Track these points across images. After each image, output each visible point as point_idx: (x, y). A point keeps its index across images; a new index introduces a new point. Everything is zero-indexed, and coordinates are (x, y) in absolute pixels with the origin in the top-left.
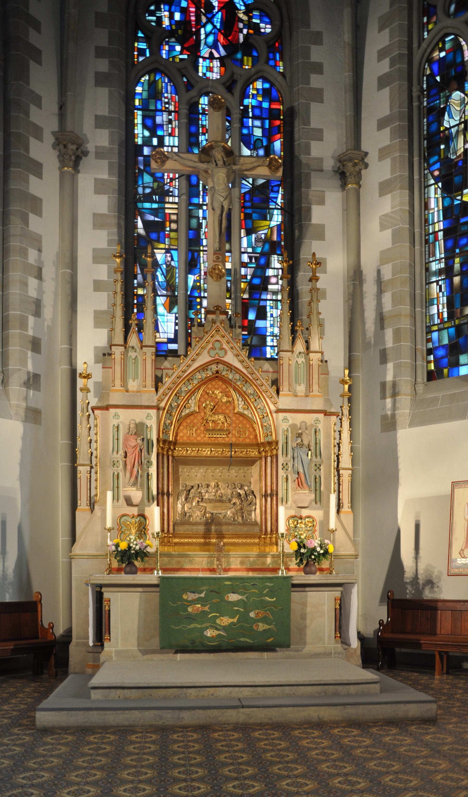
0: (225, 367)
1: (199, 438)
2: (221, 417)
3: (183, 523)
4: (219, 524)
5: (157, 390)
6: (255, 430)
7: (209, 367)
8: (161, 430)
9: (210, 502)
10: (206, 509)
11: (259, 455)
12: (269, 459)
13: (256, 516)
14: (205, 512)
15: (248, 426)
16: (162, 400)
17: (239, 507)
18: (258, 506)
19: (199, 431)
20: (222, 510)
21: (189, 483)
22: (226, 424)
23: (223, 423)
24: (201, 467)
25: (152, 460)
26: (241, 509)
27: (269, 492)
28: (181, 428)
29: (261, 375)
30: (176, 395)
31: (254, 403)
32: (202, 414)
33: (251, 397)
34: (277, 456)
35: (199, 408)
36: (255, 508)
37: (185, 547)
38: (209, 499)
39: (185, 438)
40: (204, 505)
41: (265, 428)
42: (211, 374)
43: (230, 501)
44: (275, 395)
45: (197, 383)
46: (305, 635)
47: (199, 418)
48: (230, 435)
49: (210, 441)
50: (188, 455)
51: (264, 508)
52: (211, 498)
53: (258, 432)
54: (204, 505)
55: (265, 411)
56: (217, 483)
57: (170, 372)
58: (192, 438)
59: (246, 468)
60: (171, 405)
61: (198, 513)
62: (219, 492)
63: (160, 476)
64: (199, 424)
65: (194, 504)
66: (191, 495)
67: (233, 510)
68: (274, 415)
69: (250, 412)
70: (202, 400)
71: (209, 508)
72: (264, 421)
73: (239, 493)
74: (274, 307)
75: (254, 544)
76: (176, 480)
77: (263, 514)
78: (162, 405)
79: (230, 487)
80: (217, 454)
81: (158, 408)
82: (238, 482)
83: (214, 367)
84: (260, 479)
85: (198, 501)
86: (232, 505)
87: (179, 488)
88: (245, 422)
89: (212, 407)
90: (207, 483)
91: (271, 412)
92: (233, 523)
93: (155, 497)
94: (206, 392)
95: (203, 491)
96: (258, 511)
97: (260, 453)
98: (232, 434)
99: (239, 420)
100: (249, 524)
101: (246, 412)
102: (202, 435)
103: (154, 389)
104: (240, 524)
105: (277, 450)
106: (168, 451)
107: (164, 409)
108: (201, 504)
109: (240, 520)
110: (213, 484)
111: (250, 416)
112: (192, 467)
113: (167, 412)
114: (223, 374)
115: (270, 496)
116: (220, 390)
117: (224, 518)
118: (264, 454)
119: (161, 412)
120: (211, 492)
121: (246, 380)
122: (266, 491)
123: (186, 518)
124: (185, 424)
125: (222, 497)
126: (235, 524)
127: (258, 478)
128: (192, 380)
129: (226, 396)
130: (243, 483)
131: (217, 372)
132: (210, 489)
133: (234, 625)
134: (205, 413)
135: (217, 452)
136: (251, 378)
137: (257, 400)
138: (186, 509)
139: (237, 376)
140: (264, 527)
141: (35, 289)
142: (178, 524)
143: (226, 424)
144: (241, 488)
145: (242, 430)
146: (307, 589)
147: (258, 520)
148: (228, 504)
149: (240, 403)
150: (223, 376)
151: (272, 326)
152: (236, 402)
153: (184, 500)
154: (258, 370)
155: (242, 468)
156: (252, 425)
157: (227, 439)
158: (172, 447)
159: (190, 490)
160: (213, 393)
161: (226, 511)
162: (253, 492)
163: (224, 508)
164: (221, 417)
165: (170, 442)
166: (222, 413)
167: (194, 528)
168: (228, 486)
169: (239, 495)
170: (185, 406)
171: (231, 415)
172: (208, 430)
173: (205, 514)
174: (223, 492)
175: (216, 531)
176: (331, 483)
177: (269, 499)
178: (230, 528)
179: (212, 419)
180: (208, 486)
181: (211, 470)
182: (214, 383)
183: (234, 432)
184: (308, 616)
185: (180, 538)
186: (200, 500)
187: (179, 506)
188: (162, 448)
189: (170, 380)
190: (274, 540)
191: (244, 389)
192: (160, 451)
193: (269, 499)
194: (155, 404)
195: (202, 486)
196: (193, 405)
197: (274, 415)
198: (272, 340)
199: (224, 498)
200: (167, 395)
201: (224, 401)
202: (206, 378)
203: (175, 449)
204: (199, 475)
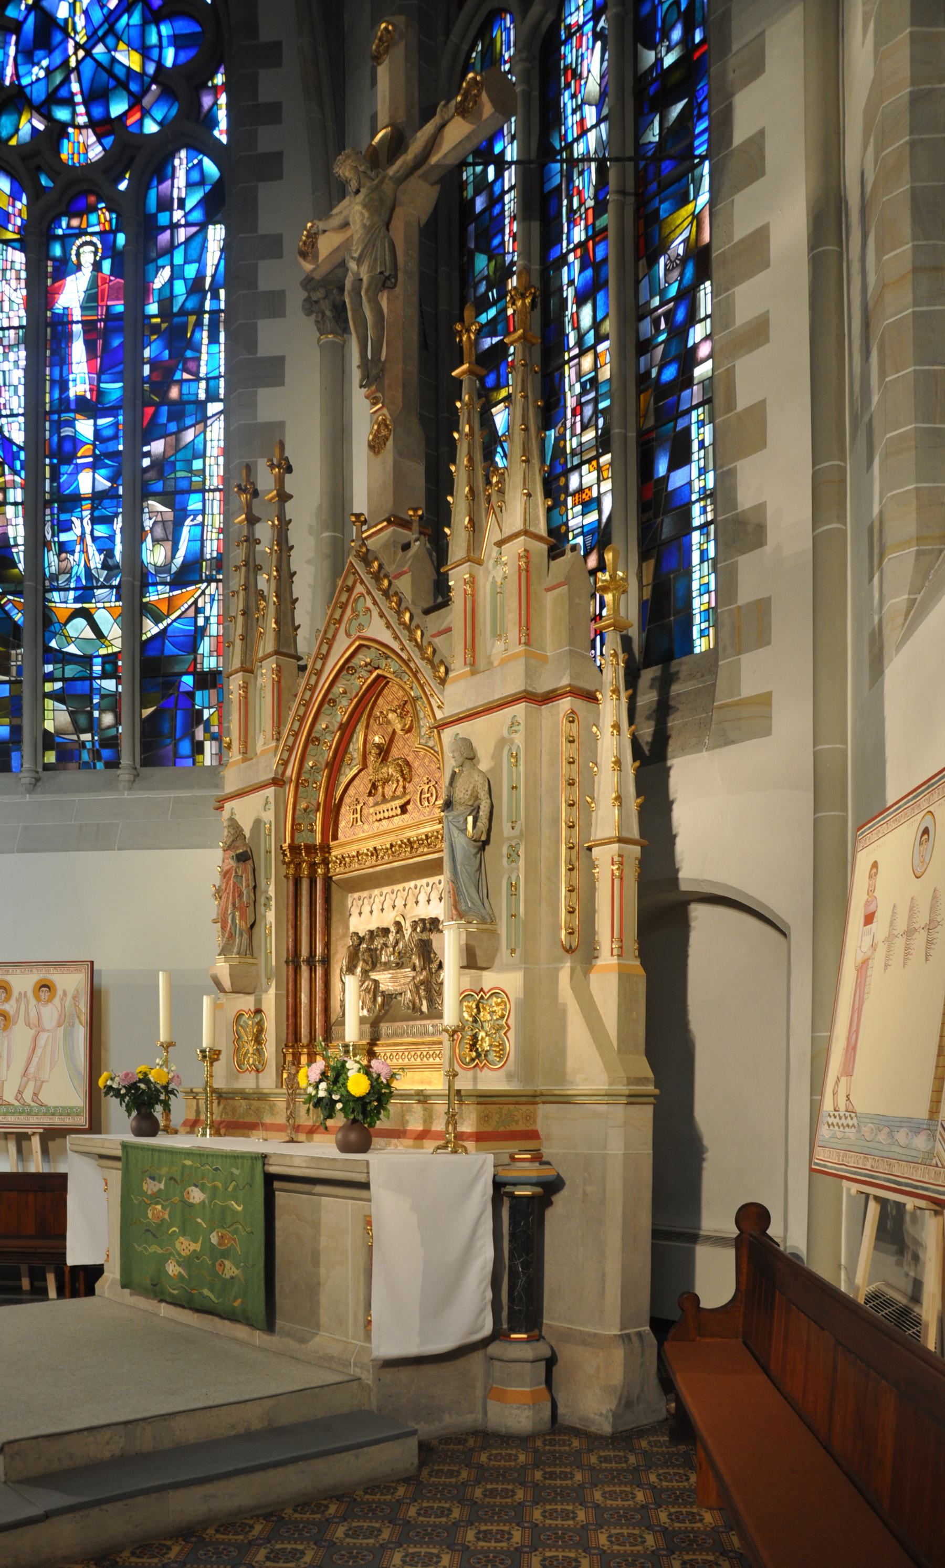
46: (318, 1303)
74: (707, 421)
81: (278, 782)
133: (198, 1258)
141: (309, 585)
146: (319, 1189)
151: (703, 471)
176: (558, 890)
184: (323, 1259)
198: (704, 511)
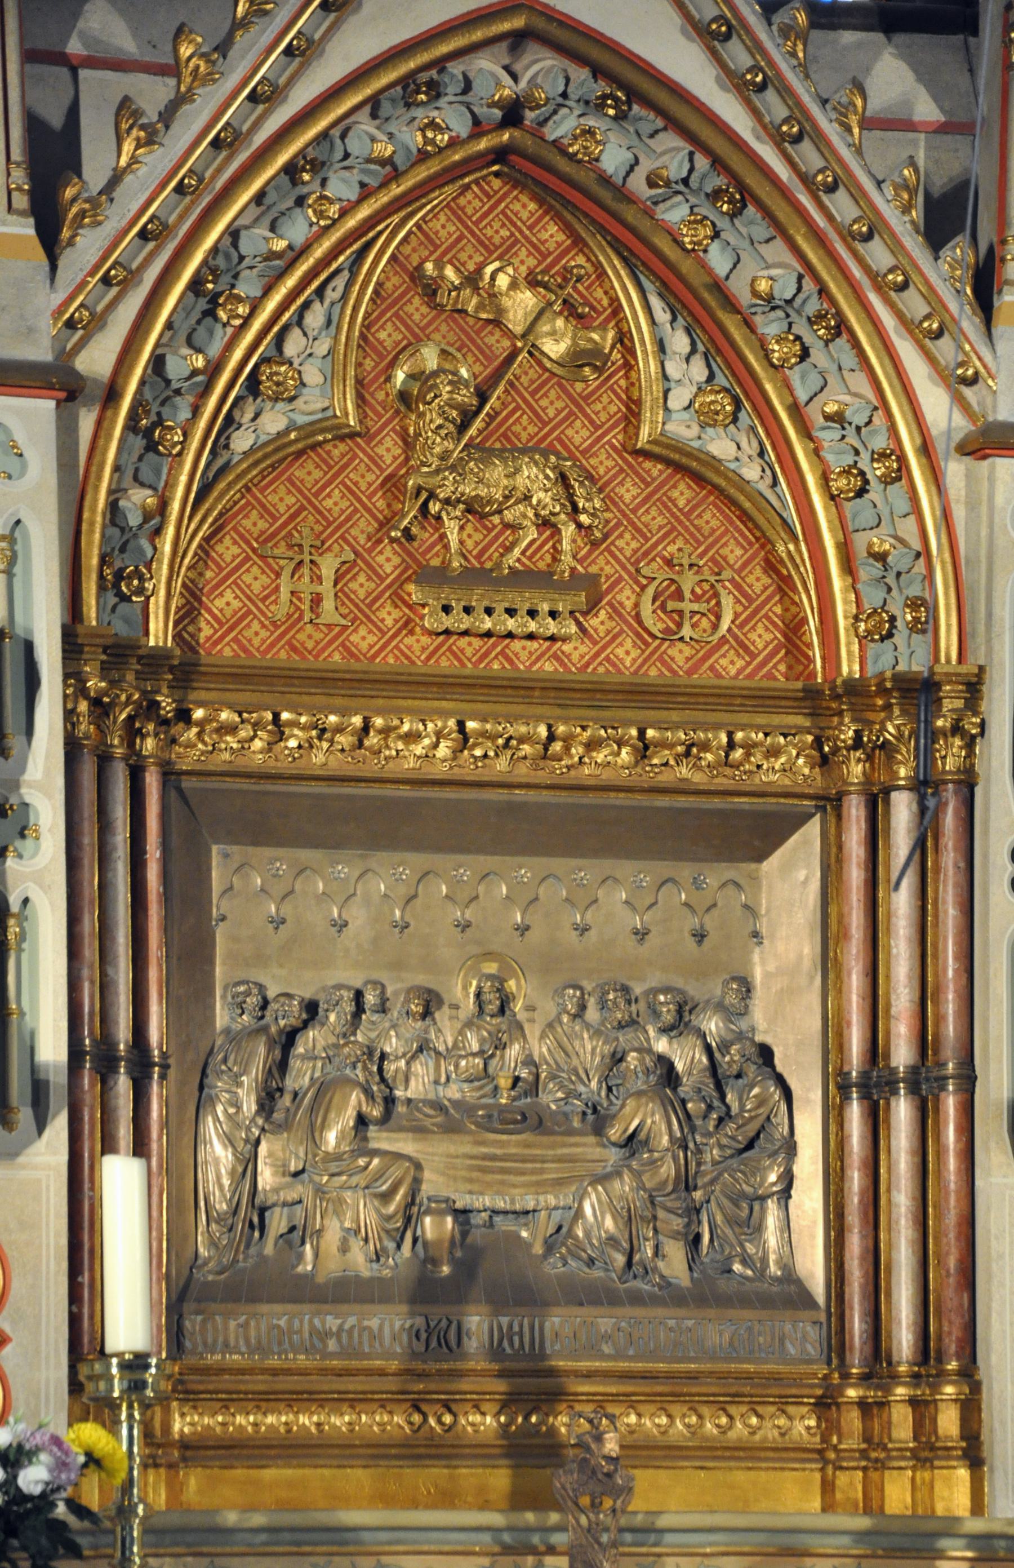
0: (581, 74)
1: (363, 639)
2: (533, 477)
3: (243, 1289)
4: (523, 1295)
5: (50, 239)
6: (784, 586)
7: (456, 68)
8: (92, 560)
9: (451, 1129)
10: (417, 1181)
11: (818, 781)
12: (902, 809)
13: (799, 1232)
14: (411, 1201)
15: (734, 553)
16: (97, 322)
17: (668, 1170)
18: (809, 1164)
19: (361, 586)
20: (539, 1187)
21: (287, 982)
22: (568, 531)
23: (545, 524)
24: (380, 859)
25: (28, 794)
26: (686, 1183)
27: (902, 1055)
28: (228, 550)
29: (859, 151)
30: (196, 285)
31: (794, 376)
32: (389, 450)
33: (770, 326)
34: (968, 783)
35: (361, 400)
36: (788, 1180)
37: (269, 1474)
38: (438, 1106)
39: (256, 634)
40: (407, 1145)
41: (868, 571)
42: (461, 127)
43: (598, 1119)
44: (960, 308)
45: (352, 194)
47: (366, 478)
48: (599, 622)
49: (445, 664)
50: (284, 765)
51: (856, 1180)
52: (453, 1092)
53: (808, 604)
54: (407, 1145)
55: (880, 442)
56: (499, 981)
57: (152, 94)
58: (307, 636)
59: (714, 875)
60: (158, 362)
61: (365, 1212)
62: (514, 1051)
63: (90, 924)
64: (362, 528)
65: (331, 1138)
66: (302, 1075)
67: (624, 1186)
68: (956, 471)
69: (750, 448)
70: (387, 335)
71: (443, 1168)
72: (867, 517)
73: (665, 1063)
75: (784, 1453)
76: (192, 956)
77: (854, 1218)
78: (97, 360)
79: (592, 1014)
80: (502, 764)
81: (64, 385)
82: (654, 980)
83: (491, 76)
84: (829, 964)
85: (362, 1121)
86: (613, 1155)
87: (210, 1019)
88: (711, 519)
89: (466, 397)
90: (422, 979)
91: (926, 449)
92: (623, 1284)
93: (59, 1080)
94: (416, 275)
95: (392, 1045)
96: (809, 1199)
97: (824, 761)
98: (616, 610)
99: (667, 505)
100: (744, 1301)
101: (720, 446)
102: (389, 616)
103: (26, 229)
104: (672, 1296)
105: (970, 743)
106: (132, 733)
107: (112, 395)
108: (380, 1139)
109: (675, 1264)
110: (462, 992)
111: (751, 472)
112: (306, 855)
113: (132, 425)
114: (553, 132)
115: (914, 1089)
116: (526, 261)
117: (550, 1247)
118: (856, 771)
119: (87, 422)
120: (454, 1053)
121: (739, 189)
122: (875, 1050)
123: (269, 1249)
124: (254, 523)
125: (534, 1087)
126: (636, 1299)
127: (809, 949)
128: (317, 166)
129: (570, 309)
130: (694, 990)
131: (512, 114)
132: (445, 1032)
134: (408, 443)
135: (507, 749)
136: (783, 172)
137: (818, 355)
138: (266, 1177)
139: (671, 156)
140: (857, 1325)
142: (208, 1295)
143: (568, 531)
144: (679, 1025)
145: (688, 582)
147: (812, 1266)
148: (588, 1147)
149: (673, 369)
150: (556, 144)
152: (647, 365)
153: (249, 1105)
154: (842, 112)
155: (685, 871)
156: (765, 542)
157: (576, 650)
158: (167, 704)
159: (290, 1038)
160: (472, 280)
161: (565, 1197)
162: (766, 1053)
163: (553, 1171)
164: (533, 477)
165: (154, 662)
166: (538, 450)
167: (332, 1323)
168: (579, 1014)
169: (667, 1074)
170: (253, 385)
171: (603, 463)
172: (435, 577)
173: (409, 1217)
174: (540, 1049)
175: (495, 1352)
177: (902, 1111)
178: (605, 1324)
179: (468, 489)
180: (430, 1003)
181: (455, 883)
182: (472, 203)
183: (626, 597)
185: (230, 1400)
186: (376, 1112)
187: (219, 1155)
188: (96, 703)
189: (157, 162)
190: (948, 1422)
191: (718, 260)
192: (84, 727)
193: (902, 1111)
194: (40, 351)
195: (383, 1009)
196: (312, 375)
197: (956, 471)
199: (551, 1097)
200: (131, 278)
201: (555, 348)
202: (423, 156)
203: (184, 715)
204: (358, 916)
